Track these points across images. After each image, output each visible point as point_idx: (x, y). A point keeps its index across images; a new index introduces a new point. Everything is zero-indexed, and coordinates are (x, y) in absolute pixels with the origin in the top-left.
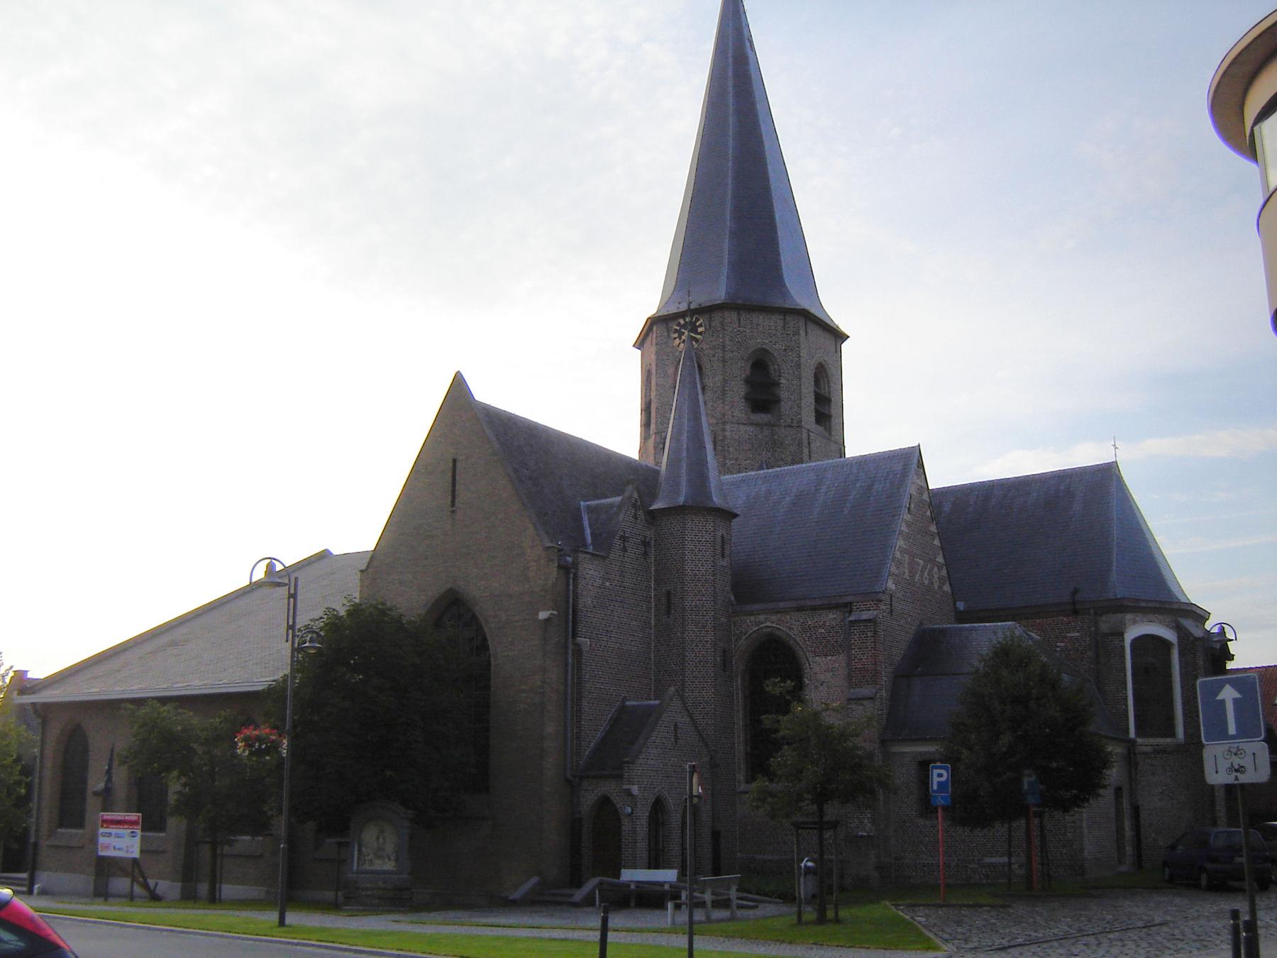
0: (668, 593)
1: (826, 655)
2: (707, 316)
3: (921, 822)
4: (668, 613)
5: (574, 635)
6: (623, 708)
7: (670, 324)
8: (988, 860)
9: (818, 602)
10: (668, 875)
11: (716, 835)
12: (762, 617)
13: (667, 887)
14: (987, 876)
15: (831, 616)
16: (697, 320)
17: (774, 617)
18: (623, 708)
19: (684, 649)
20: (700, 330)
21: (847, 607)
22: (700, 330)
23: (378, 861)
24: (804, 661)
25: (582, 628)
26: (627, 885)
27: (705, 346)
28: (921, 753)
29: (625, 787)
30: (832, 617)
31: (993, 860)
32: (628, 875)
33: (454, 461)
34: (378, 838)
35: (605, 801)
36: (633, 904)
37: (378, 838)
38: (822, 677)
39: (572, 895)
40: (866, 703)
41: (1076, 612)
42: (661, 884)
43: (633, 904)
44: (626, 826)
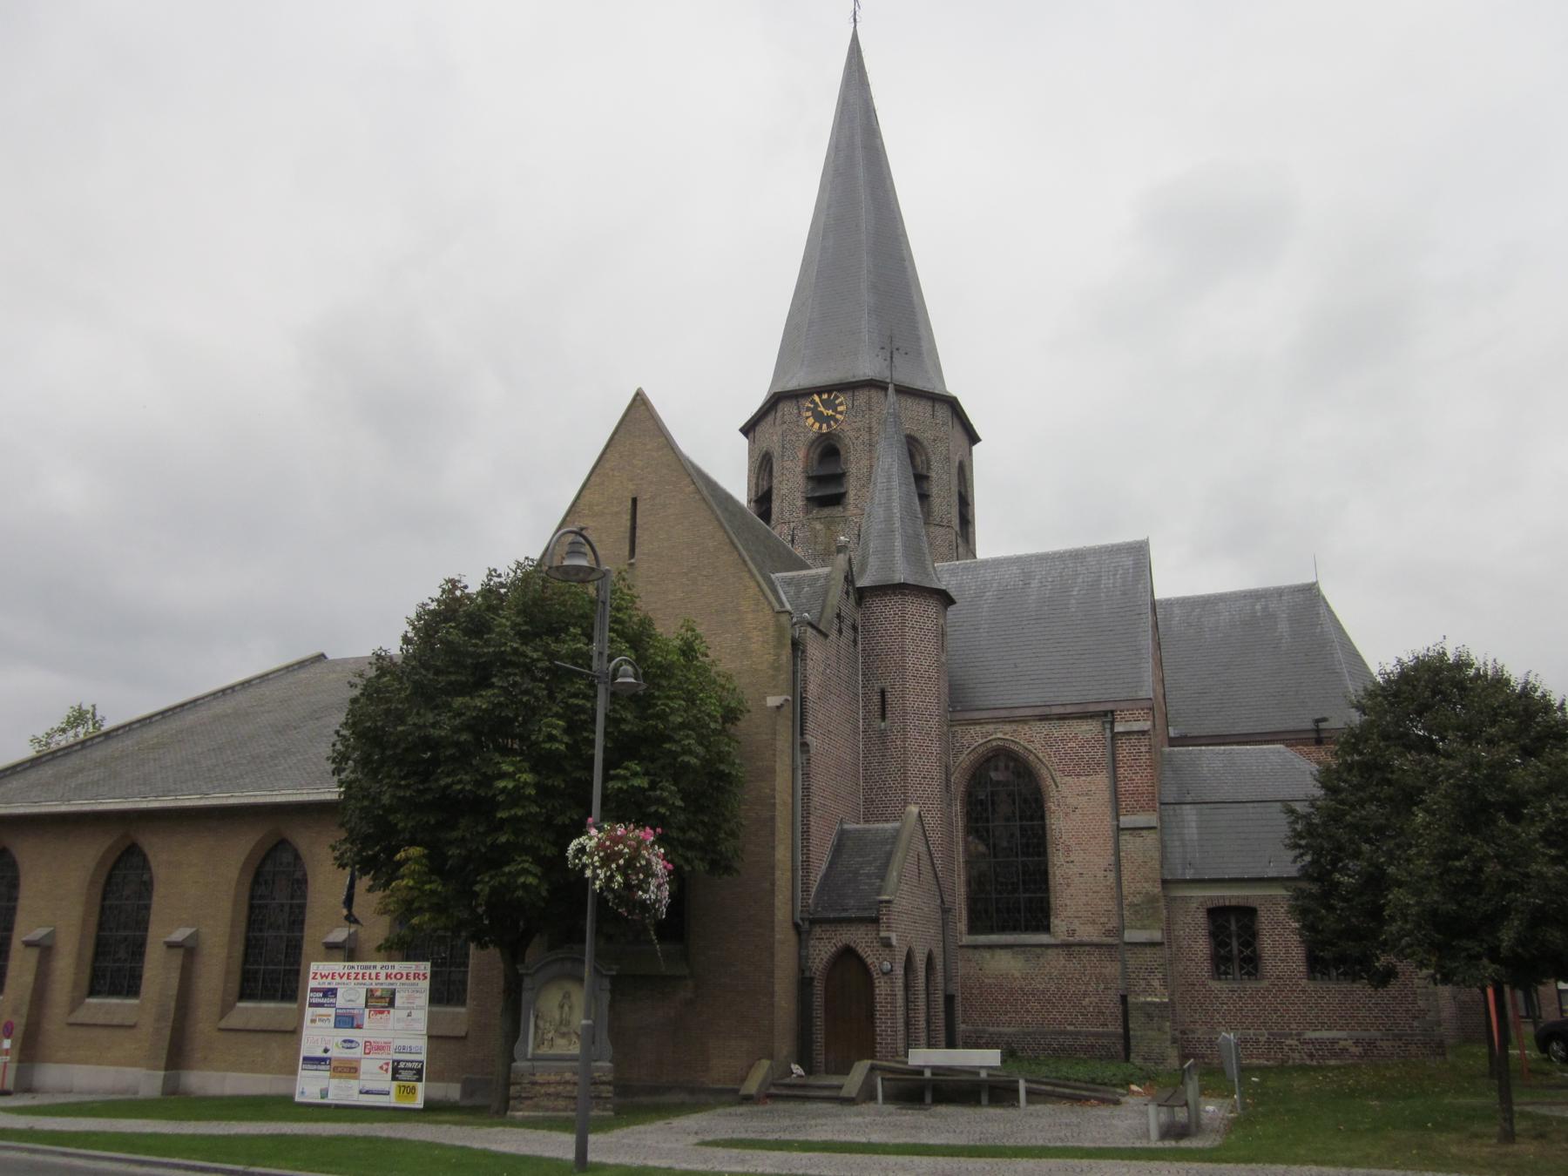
0: (883, 693)
1: (1079, 775)
2: (850, 393)
3: (1215, 985)
4: (883, 717)
5: (802, 734)
6: (842, 834)
7: (802, 401)
8: (1310, 1035)
9: (1069, 710)
10: (990, 1058)
11: (949, 999)
12: (991, 728)
13: (983, 1074)
14: (1311, 1056)
15: (1085, 727)
16: (837, 397)
17: (1007, 728)
18: (842, 834)
19: (905, 761)
20: (840, 409)
21: (1108, 716)
22: (840, 409)
23: (561, 1042)
24: (1049, 781)
25: (810, 725)
26: (919, 1071)
27: (846, 428)
28: (1211, 898)
29: (882, 934)
30: (1088, 729)
31: (1317, 1035)
32: (921, 1057)
33: (634, 501)
34: (561, 1007)
35: (848, 955)
36: (928, 1099)
37: (561, 1007)
38: (1072, 801)
39: (840, 1087)
40: (1144, 833)
41: (1319, 742)
42: (973, 1071)
43: (928, 1099)
44: (881, 988)
